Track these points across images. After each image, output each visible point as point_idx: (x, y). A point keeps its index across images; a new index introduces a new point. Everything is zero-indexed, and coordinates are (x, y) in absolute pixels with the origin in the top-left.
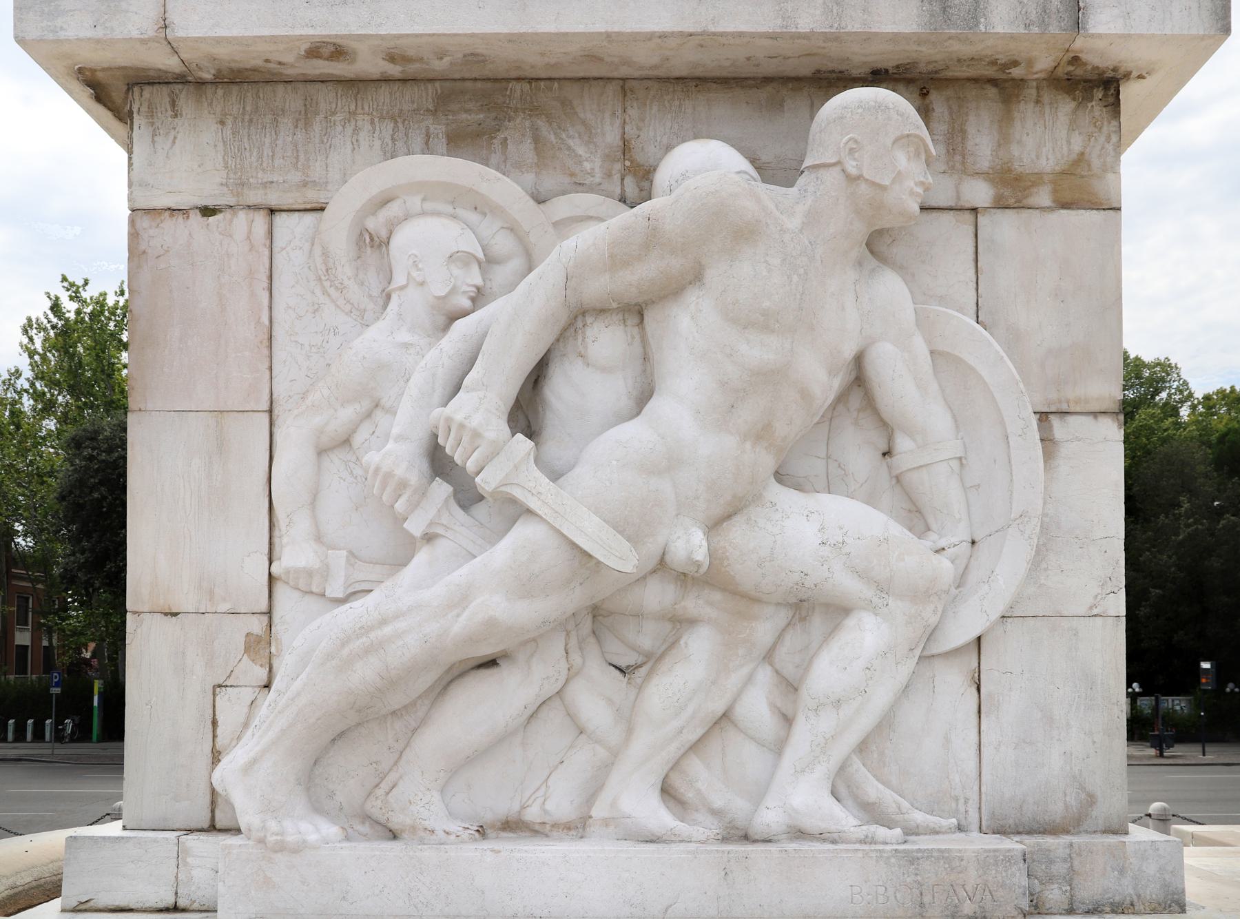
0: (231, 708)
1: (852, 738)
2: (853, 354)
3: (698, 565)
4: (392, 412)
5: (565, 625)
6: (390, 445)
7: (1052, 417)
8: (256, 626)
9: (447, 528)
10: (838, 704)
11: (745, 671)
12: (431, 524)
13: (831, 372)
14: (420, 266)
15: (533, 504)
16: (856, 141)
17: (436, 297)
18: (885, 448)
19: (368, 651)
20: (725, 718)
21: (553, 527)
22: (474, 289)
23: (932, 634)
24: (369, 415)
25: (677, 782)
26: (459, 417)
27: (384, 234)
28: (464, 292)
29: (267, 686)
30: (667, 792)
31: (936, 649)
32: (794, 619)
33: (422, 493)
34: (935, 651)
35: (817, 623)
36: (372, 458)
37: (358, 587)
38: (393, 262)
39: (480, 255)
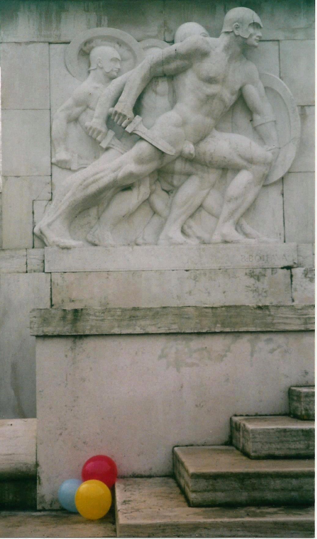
0: (38, 209)
1: (241, 210)
2: (239, 88)
3: (192, 155)
4: (94, 110)
5: (151, 175)
7: (306, 107)
8: (48, 179)
9: (113, 145)
10: (236, 199)
12: (109, 144)
13: (232, 94)
14: (101, 62)
15: (143, 136)
16: (237, 25)
18: (251, 119)
19: (93, 182)
20: (201, 207)
21: (150, 143)
23: (266, 177)
24: (85, 110)
25: (186, 227)
26: (119, 111)
27: (88, 52)
28: (115, 71)
29: (51, 200)
30: (183, 232)
33: (106, 134)
34: (268, 183)
36: (88, 124)
37: (83, 166)
38: (91, 60)
39: (120, 58)
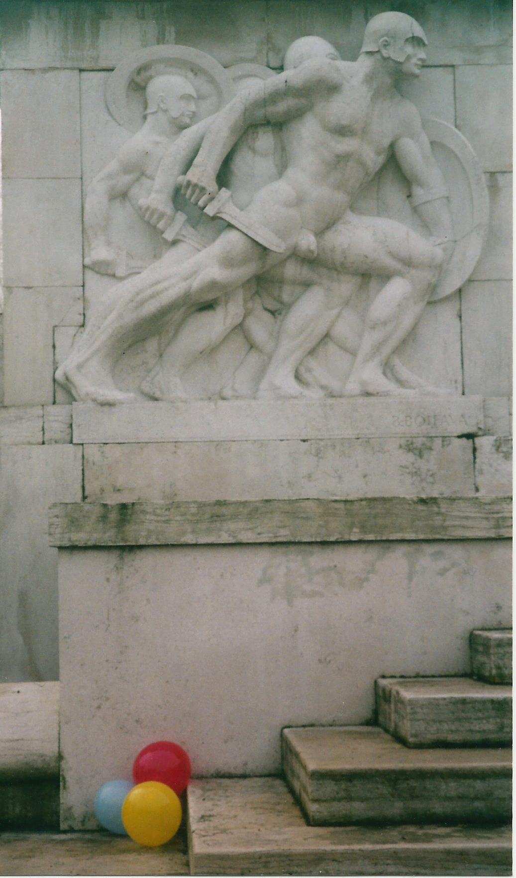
0: (63, 340)
1: (392, 343)
2: (389, 144)
3: (312, 252)
4: (152, 178)
5: (246, 284)
6: (153, 195)
7: (497, 174)
10: (385, 324)
11: (335, 312)
12: (177, 234)
13: (378, 153)
16: (387, 41)
17: (172, 118)
18: (408, 194)
19: (152, 296)
21: (243, 233)
22: (191, 113)
23: (433, 288)
24: (138, 179)
25: (302, 370)
26: (194, 180)
27: (143, 84)
29: (83, 326)
30: (298, 377)
31: (436, 298)
32: (378, 439)
33: (172, 219)
35: (373, 284)
36: (143, 202)
37: (134, 271)
39: (195, 95)
